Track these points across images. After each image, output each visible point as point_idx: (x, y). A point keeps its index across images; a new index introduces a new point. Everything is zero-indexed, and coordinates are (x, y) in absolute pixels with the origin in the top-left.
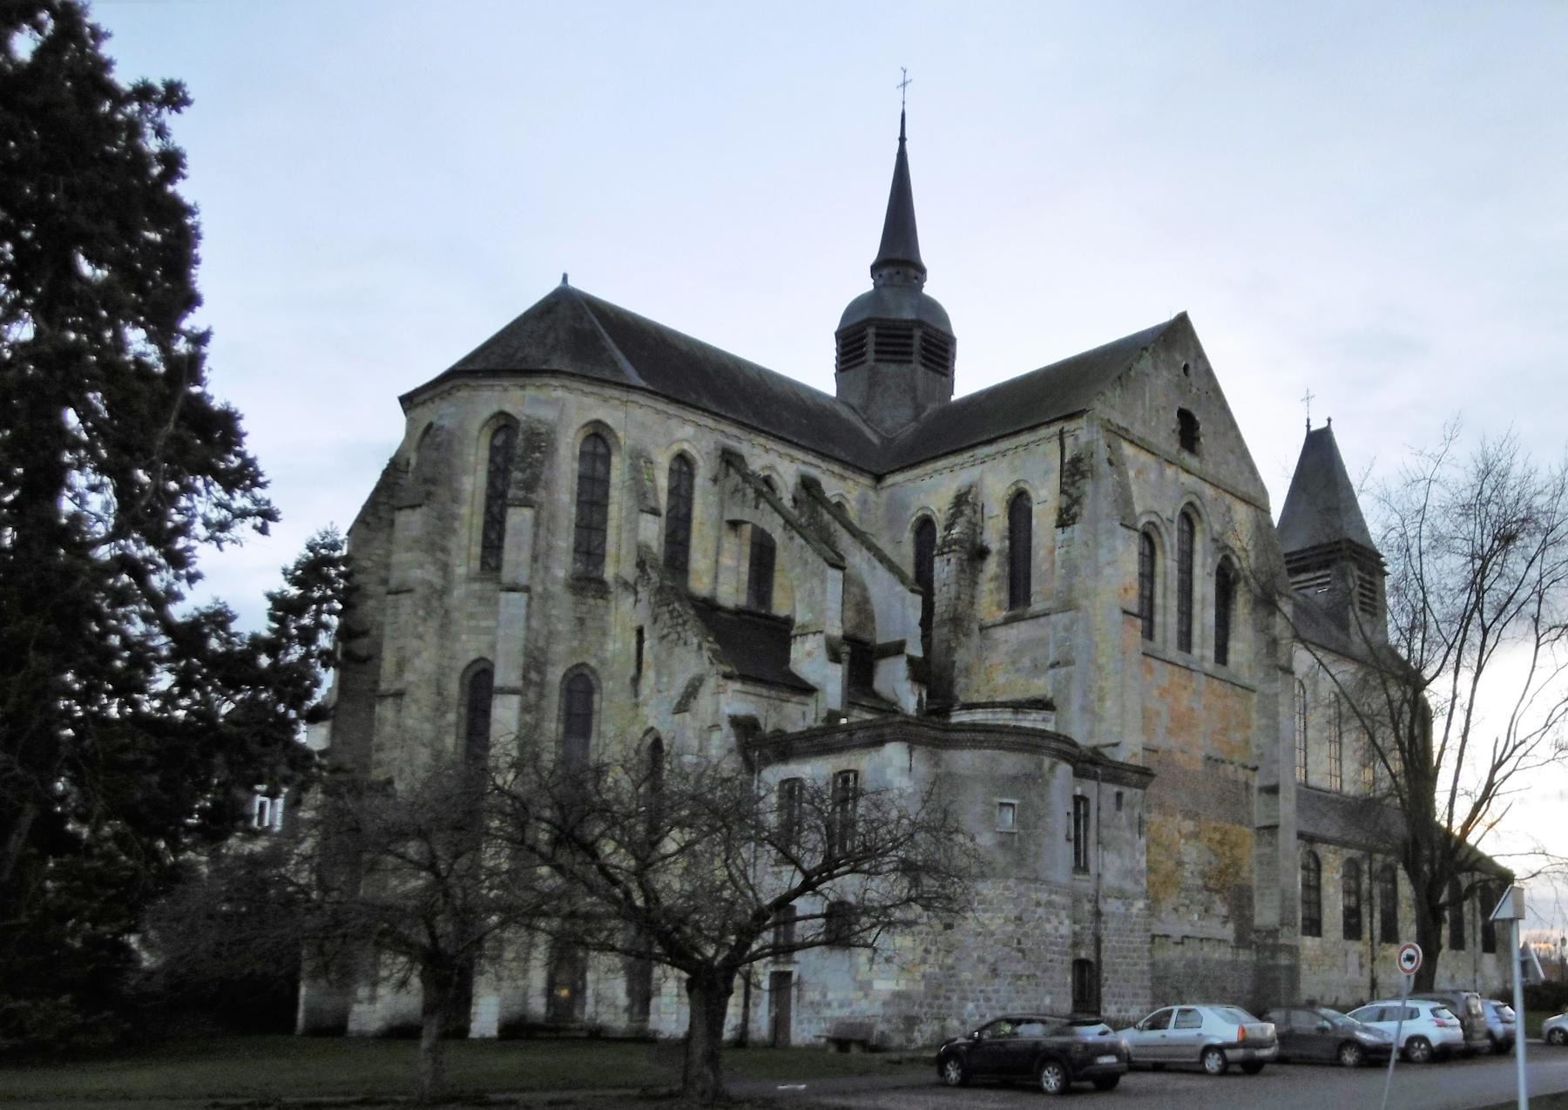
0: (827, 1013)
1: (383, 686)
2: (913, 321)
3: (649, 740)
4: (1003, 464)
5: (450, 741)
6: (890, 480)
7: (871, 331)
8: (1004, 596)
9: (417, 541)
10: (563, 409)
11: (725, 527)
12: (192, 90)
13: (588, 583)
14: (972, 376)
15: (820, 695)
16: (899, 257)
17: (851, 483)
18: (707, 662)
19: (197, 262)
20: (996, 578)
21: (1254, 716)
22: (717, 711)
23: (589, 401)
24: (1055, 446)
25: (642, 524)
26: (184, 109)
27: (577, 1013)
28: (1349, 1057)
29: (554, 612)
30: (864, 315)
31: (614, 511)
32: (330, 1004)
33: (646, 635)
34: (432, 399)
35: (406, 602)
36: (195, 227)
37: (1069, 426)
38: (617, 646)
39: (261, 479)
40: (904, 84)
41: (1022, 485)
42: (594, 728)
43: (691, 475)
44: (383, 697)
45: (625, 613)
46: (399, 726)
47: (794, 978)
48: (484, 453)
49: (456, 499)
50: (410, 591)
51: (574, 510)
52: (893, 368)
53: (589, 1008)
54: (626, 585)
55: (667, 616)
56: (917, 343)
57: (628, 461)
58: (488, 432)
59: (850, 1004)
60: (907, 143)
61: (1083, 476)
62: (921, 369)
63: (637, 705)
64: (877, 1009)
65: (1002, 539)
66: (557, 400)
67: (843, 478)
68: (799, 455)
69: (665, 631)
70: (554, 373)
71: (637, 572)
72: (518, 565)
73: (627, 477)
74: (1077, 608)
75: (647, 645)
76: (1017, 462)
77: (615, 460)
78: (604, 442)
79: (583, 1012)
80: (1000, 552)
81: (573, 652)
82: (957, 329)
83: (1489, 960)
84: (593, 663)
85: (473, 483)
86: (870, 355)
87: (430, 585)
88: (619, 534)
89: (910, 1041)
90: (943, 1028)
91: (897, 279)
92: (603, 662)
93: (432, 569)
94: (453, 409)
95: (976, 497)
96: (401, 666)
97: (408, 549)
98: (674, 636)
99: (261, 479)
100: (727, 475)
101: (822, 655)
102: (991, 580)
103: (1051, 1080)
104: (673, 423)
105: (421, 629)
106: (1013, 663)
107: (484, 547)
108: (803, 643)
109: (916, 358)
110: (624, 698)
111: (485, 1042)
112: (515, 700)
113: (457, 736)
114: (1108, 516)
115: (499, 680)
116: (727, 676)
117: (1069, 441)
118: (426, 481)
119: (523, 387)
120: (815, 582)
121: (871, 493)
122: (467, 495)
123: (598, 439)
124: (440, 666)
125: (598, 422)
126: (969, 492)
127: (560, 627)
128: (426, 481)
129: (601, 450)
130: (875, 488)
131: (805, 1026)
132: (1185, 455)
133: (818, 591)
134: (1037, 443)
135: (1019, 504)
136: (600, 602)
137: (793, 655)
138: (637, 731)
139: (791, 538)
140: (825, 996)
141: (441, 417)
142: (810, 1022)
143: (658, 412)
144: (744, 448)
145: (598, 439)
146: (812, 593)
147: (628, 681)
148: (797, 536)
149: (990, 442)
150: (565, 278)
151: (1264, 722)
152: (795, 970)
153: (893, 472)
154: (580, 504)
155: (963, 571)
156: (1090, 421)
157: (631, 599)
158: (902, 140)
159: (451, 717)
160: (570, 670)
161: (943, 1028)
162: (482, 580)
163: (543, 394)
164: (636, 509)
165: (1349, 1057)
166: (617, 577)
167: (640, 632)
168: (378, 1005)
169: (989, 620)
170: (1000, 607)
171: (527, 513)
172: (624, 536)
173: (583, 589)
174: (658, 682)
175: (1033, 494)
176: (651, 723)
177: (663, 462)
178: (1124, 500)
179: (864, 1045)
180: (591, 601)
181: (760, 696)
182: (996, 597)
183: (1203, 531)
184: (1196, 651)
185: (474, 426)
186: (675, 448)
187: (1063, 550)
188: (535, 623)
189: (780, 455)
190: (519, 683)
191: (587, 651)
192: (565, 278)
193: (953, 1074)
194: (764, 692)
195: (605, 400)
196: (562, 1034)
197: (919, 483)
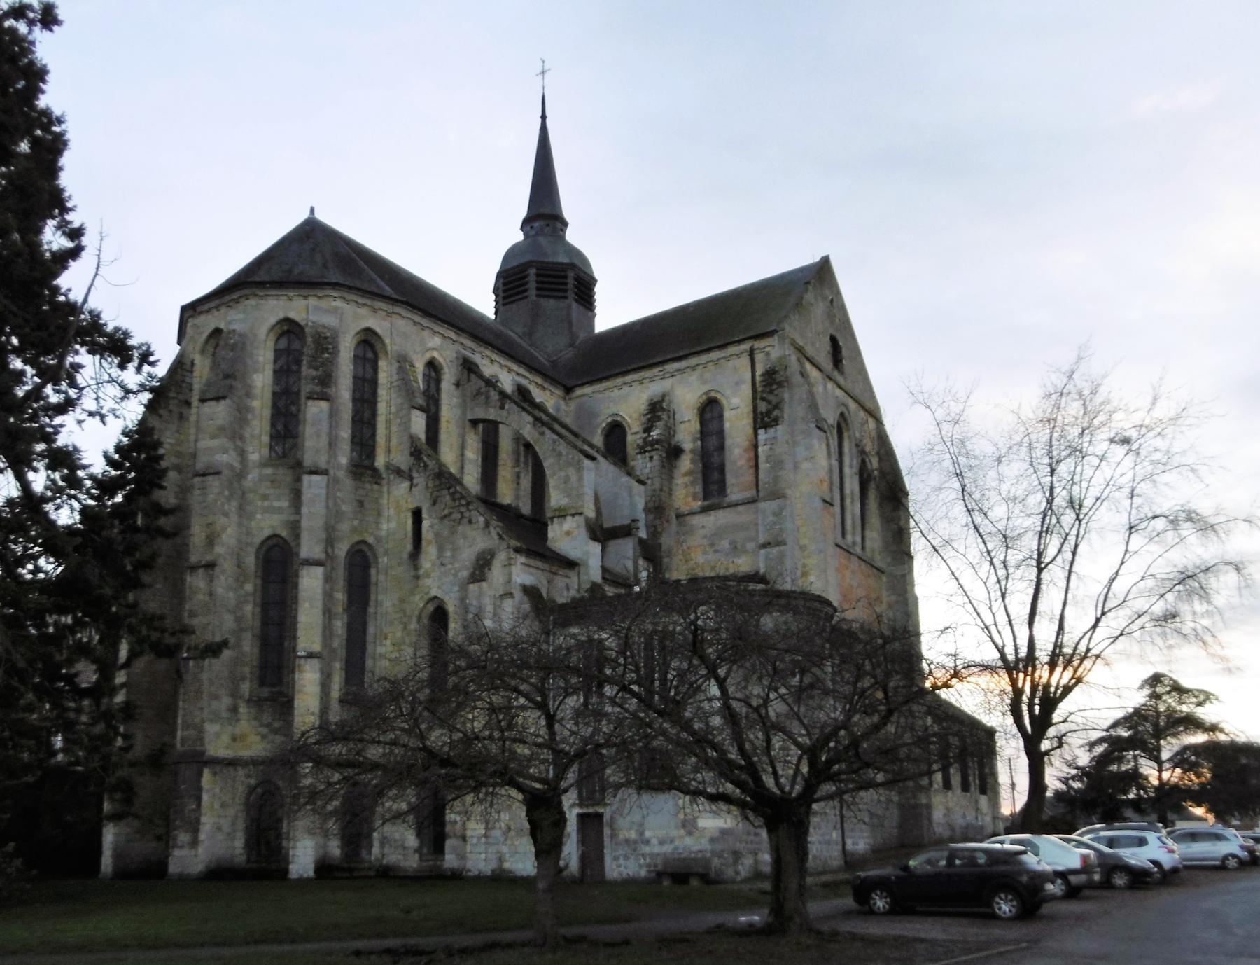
0: (647, 849)
1: (194, 559)
2: (567, 264)
3: (431, 608)
4: (693, 378)
5: (248, 608)
6: (579, 392)
7: (533, 271)
8: (699, 488)
9: (222, 429)
10: (342, 316)
11: (468, 424)
12: (61, 13)
13: (364, 467)
14: (612, 311)
15: (582, 570)
16: (544, 211)
17: (548, 393)
18: (496, 537)
19: (61, 169)
20: (690, 473)
21: (884, 593)
22: (510, 581)
23: (363, 311)
24: (745, 361)
25: (414, 419)
26: (55, 28)
27: (364, 853)
28: (1120, 880)
29: (339, 494)
30: (528, 257)
31: (382, 407)
32: (145, 848)
33: (424, 515)
34: (217, 308)
35: (214, 483)
36: (62, 135)
37: (757, 344)
38: (392, 524)
39: (152, 359)
40: (543, 72)
41: (713, 394)
42: (373, 597)
43: (438, 381)
44: (194, 568)
45: (398, 500)
46: (211, 594)
47: (606, 818)
48: (270, 355)
49: (248, 395)
50: (218, 473)
51: (350, 405)
52: (552, 302)
53: (376, 850)
54: (398, 472)
55: (448, 497)
56: (571, 281)
57: (396, 365)
58: (273, 337)
59: (672, 842)
60: (548, 120)
61: (780, 385)
62: (574, 305)
63: (417, 577)
64: (704, 844)
65: (694, 440)
66: (337, 309)
67: (544, 389)
68: (515, 367)
69: (446, 512)
70: (335, 285)
71: (412, 460)
72: (318, 451)
73: (395, 377)
74: (784, 496)
75: (426, 524)
76: (707, 375)
77: (382, 364)
78: (372, 347)
79: (370, 853)
80: (692, 451)
81: (354, 530)
82: (597, 273)
83: (984, 800)
84: (371, 540)
85: (262, 381)
86: (532, 293)
87: (231, 467)
88: (388, 428)
89: (737, 873)
90: (756, 862)
91: (547, 230)
92: (379, 539)
93: (233, 454)
94: (241, 316)
95: (670, 402)
96: (211, 541)
97: (213, 437)
98: (457, 516)
99: (152, 359)
100: (469, 380)
101: (583, 534)
102: (685, 475)
103: (1005, 907)
104: (426, 333)
105: (226, 507)
106: (712, 545)
107: (272, 437)
108: (561, 524)
109: (571, 295)
110: (401, 571)
111: (302, 882)
112: (319, 571)
113: (255, 604)
114: (803, 419)
115: (304, 552)
116: (517, 550)
117: (759, 357)
118: (227, 377)
119: (306, 297)
120: (571, 471)
121: (562, 403)
122: (257, 391)
123: (369, 343)
124: (239, 541)
125: (369, 331)
126: (662, 401)
127: (344, 508)
128: (227, 377)
129: (370, 355)
130: (564, 399)
131: (622, 861)
132: (836, 374)
133: (574, 478)
134: (727, 359)
135: (710, 409)
136: (376, 487)
137: (550, 535)
138: (418, 601)
139: (542, 434)
140: (642, 834)
141: (230, 322)
142: (626, 857)
143: (415, 323)
144: (477, 358)
145: (369, 343)
146: (567, 480)
147: (405, 556)
148: (548, 432)
149: (680, 359)
150: (312, 210)
151: (893, 598)
152: (607, 812)
153: (583, 385)
154: (354, 400)
155: (663, 467)
156: (782, 339)
157: (406, 484)
158: (544, 117)
159: (249, 587)
160: (352, 546)
161: (756, 862)
162: (272, 466)
163: (324, 304)
164: (406, 406)
165: (1120, 880)
166: (388, 466)
167: (417, 515)
168: (200, 850)
169: (685, 509)
170: (695, 498)
171: (324, 405)
172: (394, 429)
173: (362, 475)
174: (440, 555)
175: (724, 402)
176: (434, 592)
177: (420, 366)
178: (813, 407)
179: (706, 878)
180: (368, 486)
181: (538, 568)
182: (691, 489)
183: (849, 437)
184: (849, 537)
185: (262, 331)
186: (428, 356)
187: (767, 447)
188: (331, 504)
189: (502, 366)
190: (322, 556)
191: (367, 531)
192: (312, 210)
193: (880, 904)
194: (539, 564)
195: (375, 311)
196: (356, 874)
197: (607, 393)
